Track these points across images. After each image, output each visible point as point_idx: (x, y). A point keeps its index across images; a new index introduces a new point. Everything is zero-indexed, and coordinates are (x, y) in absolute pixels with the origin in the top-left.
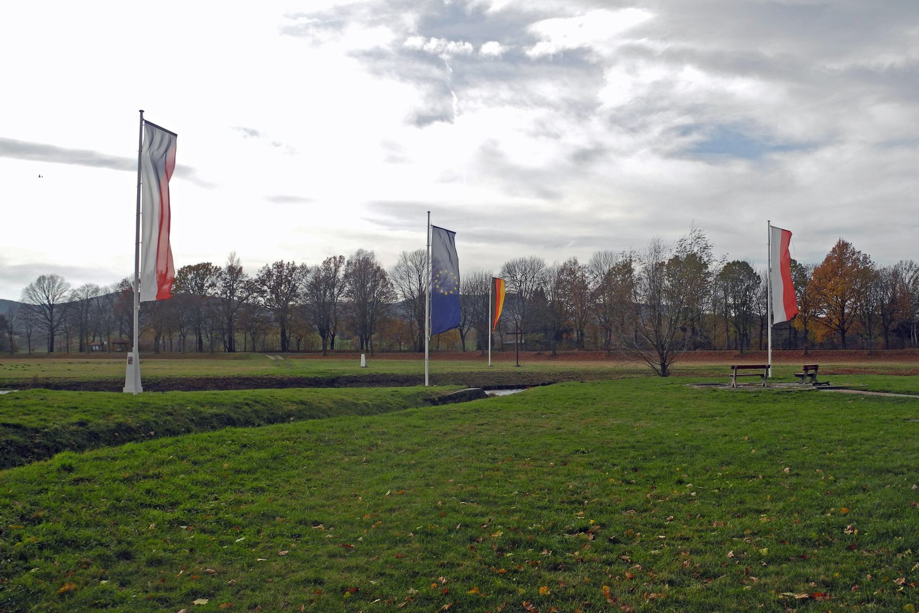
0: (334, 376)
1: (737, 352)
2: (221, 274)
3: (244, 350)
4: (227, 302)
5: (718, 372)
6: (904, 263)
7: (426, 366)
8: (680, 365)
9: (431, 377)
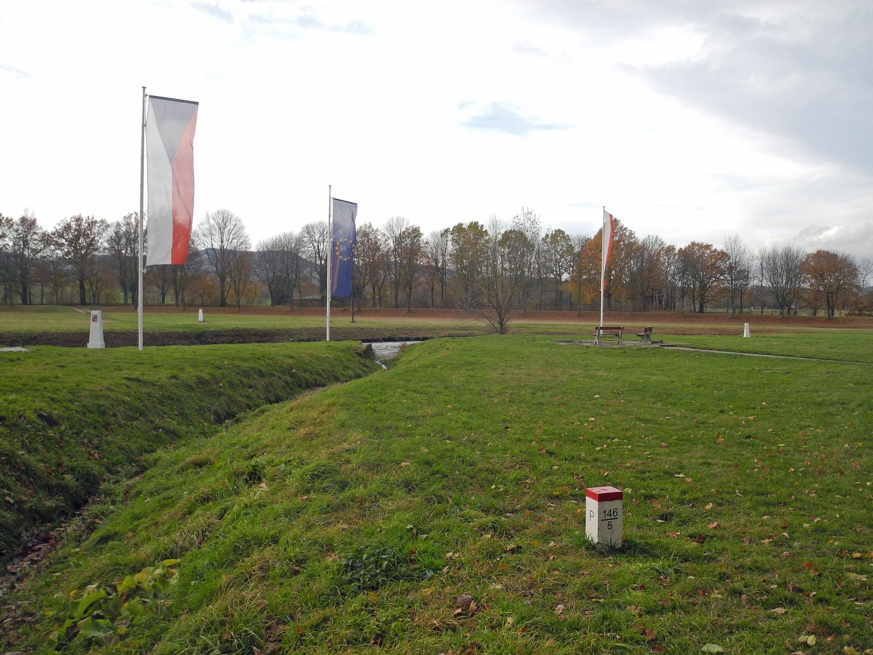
0: (200, 331)
1: (522, 312)
2: (12, 225)
3: (40, 302)
4: (17, 256)
5: (524, 330)
6: (651, 237)
7: (328, 321)
8: (758, 327)
9: (331, 333)
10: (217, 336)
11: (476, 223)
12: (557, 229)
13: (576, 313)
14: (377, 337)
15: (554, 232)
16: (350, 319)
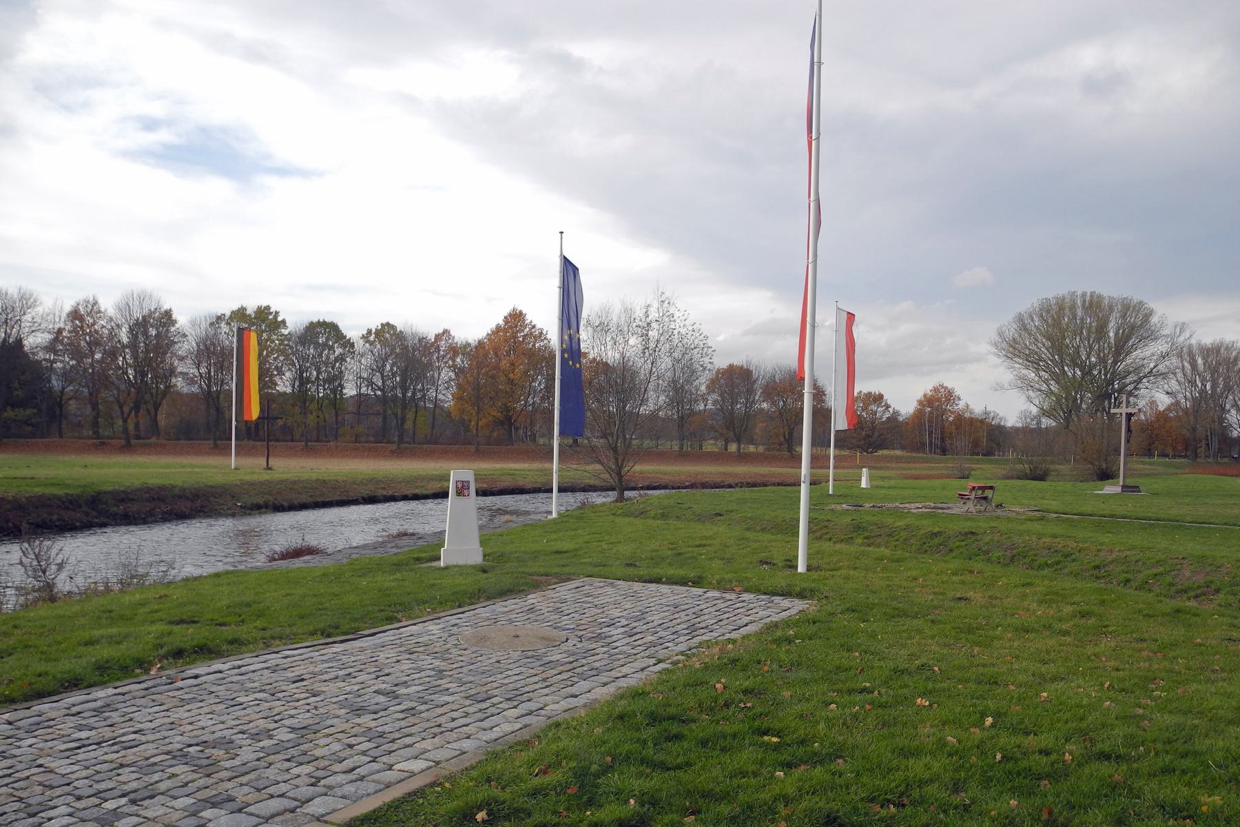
10: (122, 500)
11: (268, 308)
12: (384, 322)
13: (472, 448)
14: (352, 496)
15: (380, 327)
16: (262, 461)
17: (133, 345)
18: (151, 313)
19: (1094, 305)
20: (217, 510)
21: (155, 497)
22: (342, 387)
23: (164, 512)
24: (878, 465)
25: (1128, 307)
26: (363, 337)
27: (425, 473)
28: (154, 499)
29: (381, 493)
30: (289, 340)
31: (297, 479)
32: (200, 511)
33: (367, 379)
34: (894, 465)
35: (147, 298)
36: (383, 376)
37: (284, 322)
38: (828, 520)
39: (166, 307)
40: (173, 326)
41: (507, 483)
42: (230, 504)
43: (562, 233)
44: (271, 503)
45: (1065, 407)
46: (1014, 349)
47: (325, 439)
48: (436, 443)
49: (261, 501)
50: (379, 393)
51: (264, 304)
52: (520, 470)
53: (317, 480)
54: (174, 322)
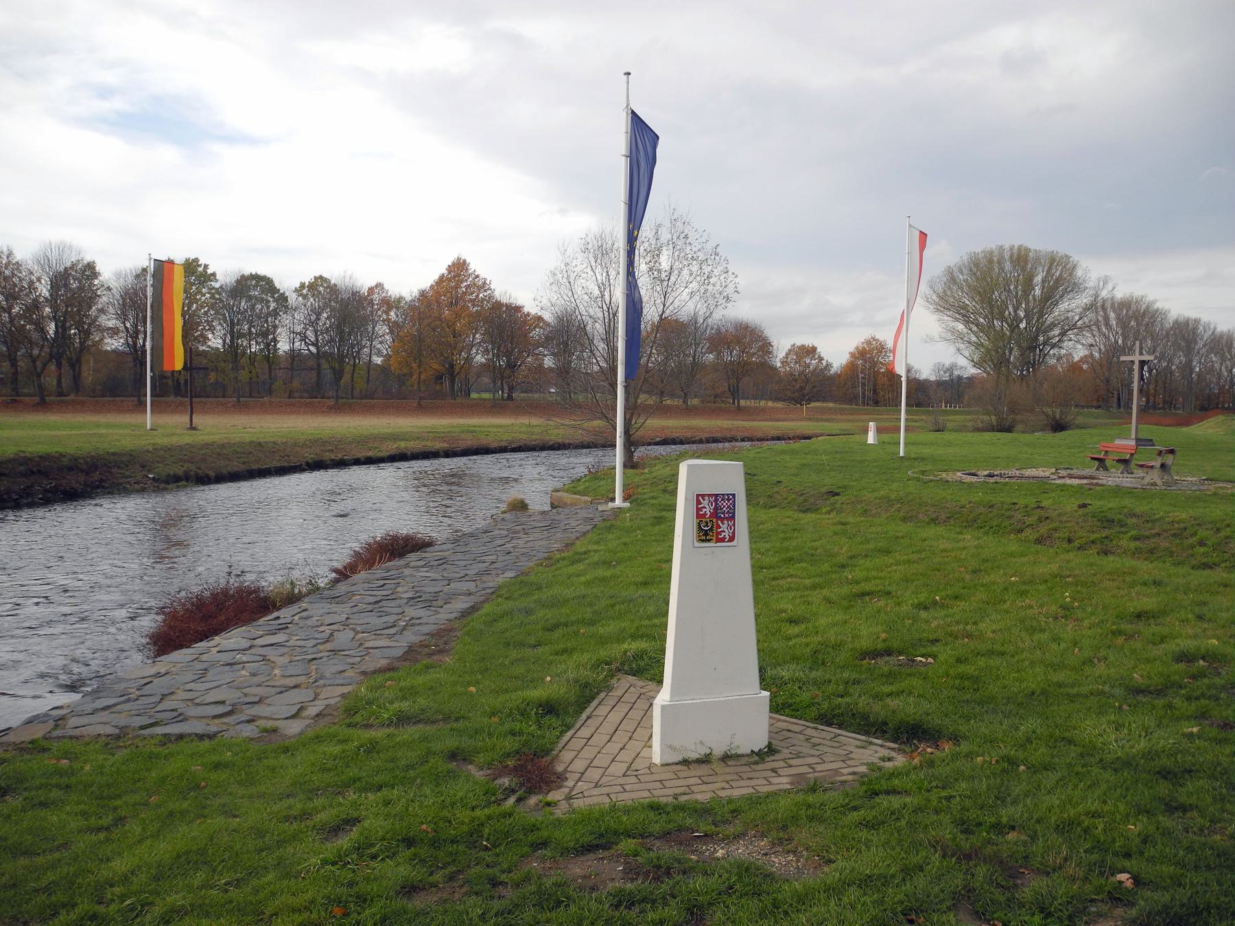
11: (196, 260)
14: (294, 461)
16: (185, 419)
17: (53, 301)
18: (73, 266)
19: (1021, 258)
20: (121, 484)
21: (35, 469)
22: (275, 340)
23: (46, 491)
24: (824, 417)
25: (1053, 261)
26: (296, 290)
27: (376, 432)
28: (33, 473)
29: (328, 456)
30: (220, 294)
31: (226, 441)
32: (98, 487)
33: (300, 334)
34: (839, 417)
35: (66, 249)
36: (316, 332)
37: (214, 274)
38: (1014, 504)
39: (88, 258)
40: (96, 278)
41: (469, 442)
42: (139, 477)
43: (629, 74)
44: (192, 473)
45: (994, 358)
46: (946, 303)
47: (257, 395)
48: (372, 398)
49: (180, 472)
50: (313, 349)
51: (193, 257)
52: (479, 427)
53: (251, 443)
54: (95, 275)
